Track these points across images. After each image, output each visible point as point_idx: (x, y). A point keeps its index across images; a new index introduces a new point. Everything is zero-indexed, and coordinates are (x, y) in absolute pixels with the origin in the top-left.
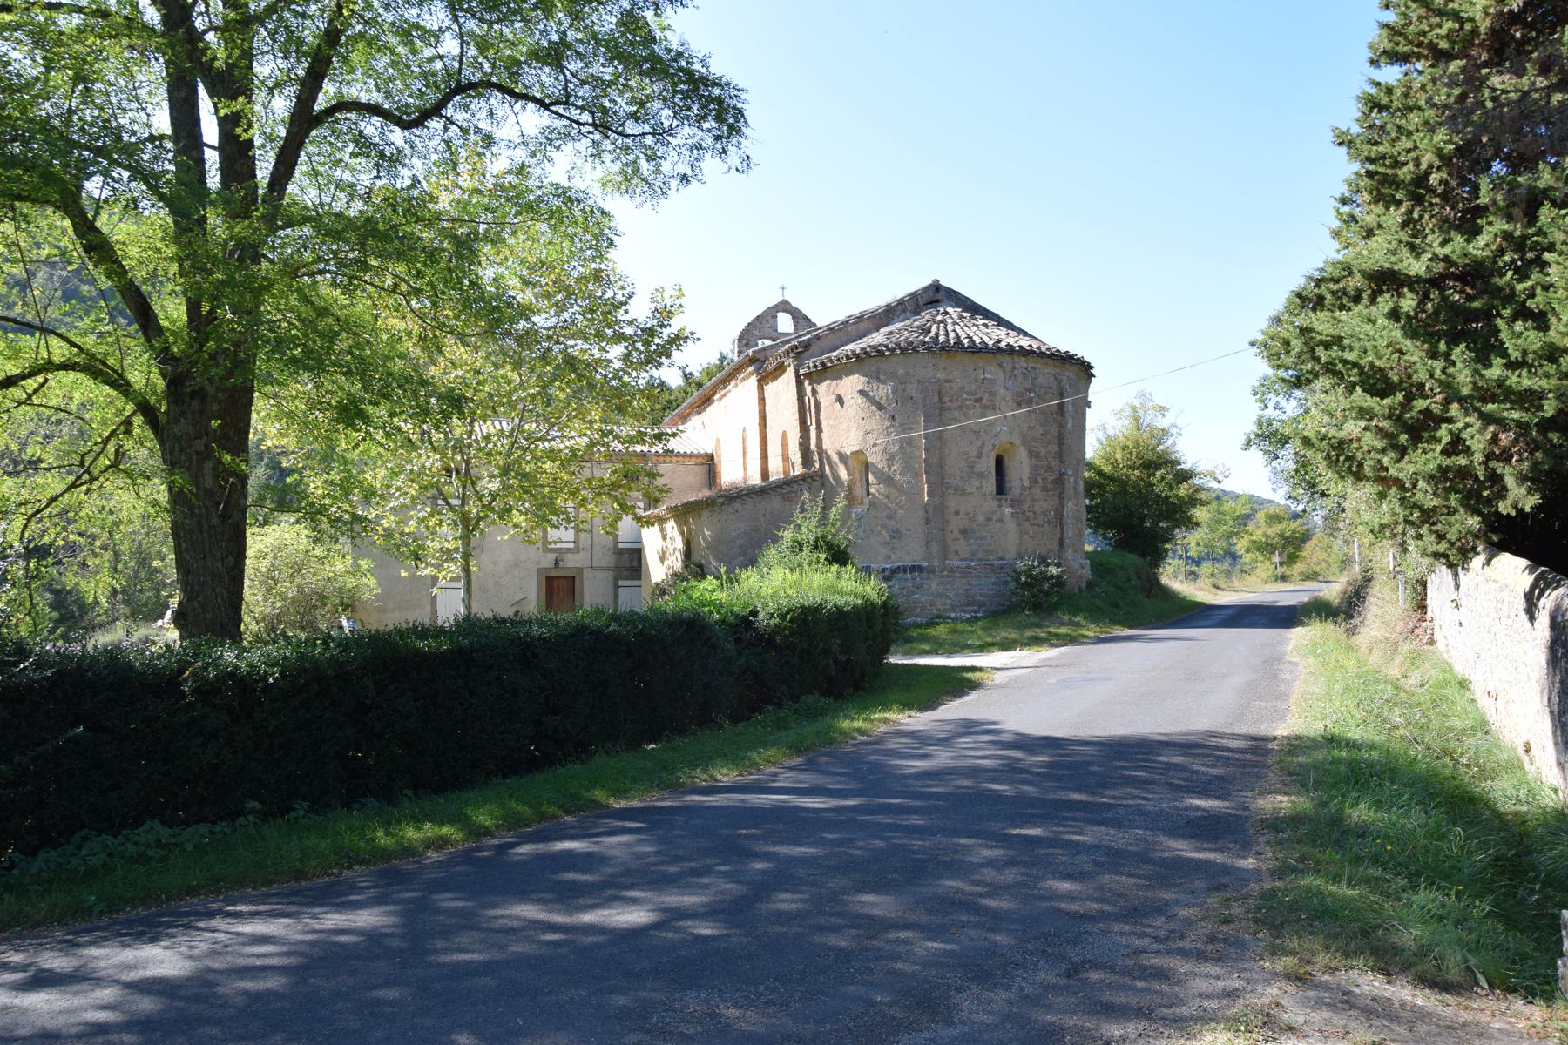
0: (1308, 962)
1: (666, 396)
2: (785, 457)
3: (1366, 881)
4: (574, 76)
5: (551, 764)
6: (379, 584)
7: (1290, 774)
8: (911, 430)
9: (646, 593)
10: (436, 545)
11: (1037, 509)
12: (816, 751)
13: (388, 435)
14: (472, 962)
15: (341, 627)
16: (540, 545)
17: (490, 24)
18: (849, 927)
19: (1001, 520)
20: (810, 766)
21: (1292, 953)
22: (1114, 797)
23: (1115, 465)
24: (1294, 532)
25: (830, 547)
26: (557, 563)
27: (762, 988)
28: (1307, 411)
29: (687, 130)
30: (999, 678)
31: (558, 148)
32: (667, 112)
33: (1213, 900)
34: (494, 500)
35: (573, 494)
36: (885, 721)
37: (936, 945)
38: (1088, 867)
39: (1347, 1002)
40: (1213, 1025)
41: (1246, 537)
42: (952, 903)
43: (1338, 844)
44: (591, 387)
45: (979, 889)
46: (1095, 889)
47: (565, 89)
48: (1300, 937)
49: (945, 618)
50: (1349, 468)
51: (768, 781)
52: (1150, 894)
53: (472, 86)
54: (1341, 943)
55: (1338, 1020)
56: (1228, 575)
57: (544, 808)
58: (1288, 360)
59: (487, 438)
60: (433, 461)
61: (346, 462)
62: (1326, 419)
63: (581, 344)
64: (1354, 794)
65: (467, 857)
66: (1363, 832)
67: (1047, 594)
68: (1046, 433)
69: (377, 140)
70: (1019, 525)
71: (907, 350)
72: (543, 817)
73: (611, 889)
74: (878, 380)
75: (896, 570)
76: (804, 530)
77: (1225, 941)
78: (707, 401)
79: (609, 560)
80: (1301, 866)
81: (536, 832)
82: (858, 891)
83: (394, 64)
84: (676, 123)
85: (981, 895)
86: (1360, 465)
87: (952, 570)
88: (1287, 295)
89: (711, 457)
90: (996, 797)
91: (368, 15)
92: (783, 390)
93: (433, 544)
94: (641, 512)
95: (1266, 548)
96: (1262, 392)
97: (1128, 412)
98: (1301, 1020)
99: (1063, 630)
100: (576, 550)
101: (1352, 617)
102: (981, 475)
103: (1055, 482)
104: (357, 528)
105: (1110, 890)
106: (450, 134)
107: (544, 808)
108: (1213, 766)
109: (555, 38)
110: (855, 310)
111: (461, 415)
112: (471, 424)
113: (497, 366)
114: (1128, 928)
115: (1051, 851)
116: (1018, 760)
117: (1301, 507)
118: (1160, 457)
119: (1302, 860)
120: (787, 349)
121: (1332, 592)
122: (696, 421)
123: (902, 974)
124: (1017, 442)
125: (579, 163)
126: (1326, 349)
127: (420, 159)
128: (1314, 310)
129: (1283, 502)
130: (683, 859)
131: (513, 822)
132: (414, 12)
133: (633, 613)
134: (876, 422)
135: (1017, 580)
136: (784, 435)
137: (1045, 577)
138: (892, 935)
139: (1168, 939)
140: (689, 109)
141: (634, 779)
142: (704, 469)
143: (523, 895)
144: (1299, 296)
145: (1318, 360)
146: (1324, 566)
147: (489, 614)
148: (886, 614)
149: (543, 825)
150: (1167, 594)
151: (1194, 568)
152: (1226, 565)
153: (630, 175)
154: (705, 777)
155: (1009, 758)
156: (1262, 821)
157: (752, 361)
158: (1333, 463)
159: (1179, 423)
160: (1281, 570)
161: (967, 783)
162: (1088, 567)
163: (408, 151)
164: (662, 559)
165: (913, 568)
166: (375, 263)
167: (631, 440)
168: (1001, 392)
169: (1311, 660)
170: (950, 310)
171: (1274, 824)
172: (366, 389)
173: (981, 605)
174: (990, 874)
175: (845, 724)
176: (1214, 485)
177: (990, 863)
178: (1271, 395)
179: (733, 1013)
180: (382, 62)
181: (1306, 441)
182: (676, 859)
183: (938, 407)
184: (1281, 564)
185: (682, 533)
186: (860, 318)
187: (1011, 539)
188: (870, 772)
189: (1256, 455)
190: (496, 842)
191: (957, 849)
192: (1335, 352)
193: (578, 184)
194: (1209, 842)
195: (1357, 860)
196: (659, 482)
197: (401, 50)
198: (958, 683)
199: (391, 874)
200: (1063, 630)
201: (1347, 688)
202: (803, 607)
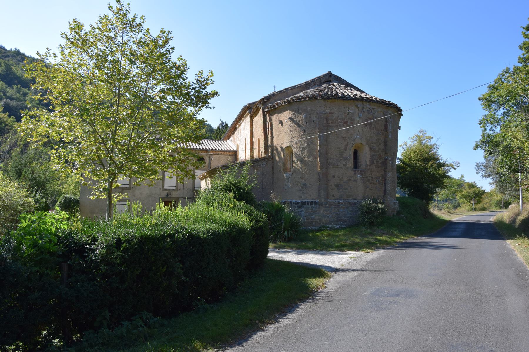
19: (355, 181)
23: (411, 160)
26: (167, 195)
70: (364, 183)
71: (312, 98)
74: (298, 113)
75: (303, 203)
92: (259, 119)
96: (483, 123)
99: (384, 238)
102: (346, 159)
124: (364, 143)
137: (376, 209)
159: (438, 143)
162: (397, 204)
165: (312, 203)
170: (335, 84)
186: (294, 87)
187: (360, 190)
200: (384, 238)
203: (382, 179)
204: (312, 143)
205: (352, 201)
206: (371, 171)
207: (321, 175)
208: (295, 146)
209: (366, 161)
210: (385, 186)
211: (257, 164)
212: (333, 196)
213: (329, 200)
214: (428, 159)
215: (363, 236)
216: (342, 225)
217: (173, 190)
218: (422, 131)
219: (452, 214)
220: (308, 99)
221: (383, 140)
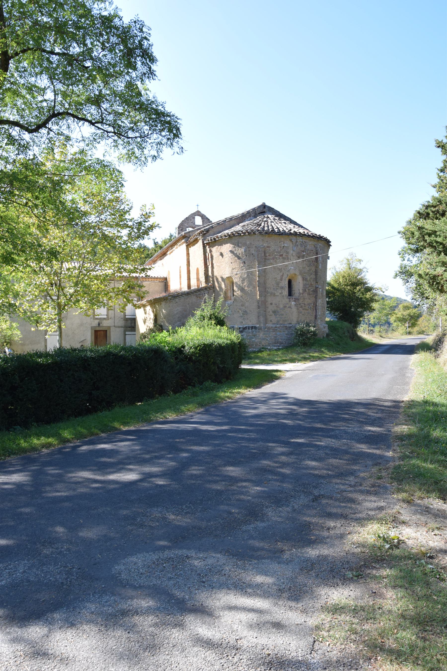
0: (412, 495)
1: (146, 252)
2: (198, 279)
3: (438, 461)
4: (105, 110)
5: (96, 411)
6: (22, 333)
7: (409, 416)
8: (252, 268)
9: (138, 338)
10: (47, 316)
11: (306, 303)
12: (208, 406)
13: (24, 268)
14: (61, 496)
15: (5, 352)
16: (92, 317)
17: (68, 86)
18: (221, 481)
19: (290, 307)
20: (207, 412)
21: (406, 491)
22: (335, 426)
23: (339, 284)
24: (415, 313)
25: (216, 318)
26: (99, 324)
27: (184, 507)
28: (421, 262)
29: (155, 136)
30: (288, 375)
31: (99, 143)
32: (147, 127)
33: (374, 470)
34: (71, 297)
35: (106, 295)
36: (239, 393)
37: (258, 488)
38: (323, 455)
39: (427, 511)
40: (372, 521)
41: (394, 315)
42: (265, 470)
43: (427, 446)
44: (114, 248)
45: (277, 465)
46: (325, 465)
47: (101, 116)
48: (409, 485)
49: (265, 349)
50: (438, 287)
51: (189, 419)
52: (348, 467)
53: (59, 114)
54: (426, 487)
55: (423, 519)
56: (387, 331)
57: (92, 430)
58: (413, 241)
59: (68, 269)
60: (45, 280)
61: (6, 281)
62: (429, 266)
63: (110, 229)
64: (434, 425)
65: (60, 451)
66: (437, 441)
67: (309, 339)
68: (310, 270)
69: (17, 138)
70: (298, 309)
71: (251, 233)
72: (92, 434)
73: (121, 465)
74: (238, 246)
75: (245, 328)
76: (205, 311)
77: (379, 486)
78: (164, 254)
79: (122, 323)
80: (411, 455)
81: (89, 441)
82: (225, 465)
83: (25, 103)
84: (150, 132)
85: (277, 467)
86: (442, 286)
87: (269, 328)
88: (414, 212)
89: (166, 279)
90: (285, 426)
91: (12, 80)
92: (197, 250)
93: (45, 317)
94: (135, 302)
95: (402, 320)
96: (402, 254)
97: (345, 261)
98: (408, 519)
99: (316, 354)
100: (107, 319)
101: (437, 350)
102: (282, 288)
103: (313, 291)
104: (11, 310)
105: (332, 465)
106: (50, 136)
107: (92, 430)
108: (377, 413)
109: (97, 93)
110: (229, 215)
111: (56, 258)
112: (62, 264)
113: (72, 239)
114: (338, 481)
115: (307, 449)
116: (295, 410)
117: (418, 303)
118: (359, 281)
119: (412, 453)
120: (199, 232)
121: (430, 339)
122: (159, 263)
123: (243, 500)
124: (298, 273)
125: (108, 149)
126: (429, 237)
127: (37, 147)
128: (425, 219)
129: (410, 301)
130: (152, 452)
131: (79, 436)
132: (33, 79)
133: (131, 347)
134: (237, 264)
135: (297, 332)
136: (198, 270)
138: (240, 484)
139: (355, 486)
140: (156, 126)
141: (131, 418)
142: (163, 284)
143: (84, 467)
144: (419, 213)
145: (426, 241)
146: (427, 328)
147: (69, 347)
148: (240, 347)
149: (92, 438)
150: (360, 339)
151: (372, 328)
152: (386, 327)
153: (130, 156)
154: (162, 417)
155: (291, 409)
156: (396, 436)
157: (184, 237)
158: (431, 285)
160: (408, 330)
161: (273, 420)
163: (32, 144)
164: (145, 322)
165: (252, 328)
166: (17, 193)
167: (131, 271)
168: (291, 252)
169: (420, 368)
170: (270, 216)
171: (401, 438)
172: (15, 247)
173: (281, 343)
174: (283, 458)
175: (222, 394)
176: (382, 293)
177: (283, 454)
178: (406, 255)
179: (172, 517)
180: (19, 102)
181: (420, 276)
182: (149, 452)
183: (264, 258)
184: (409, 327)
185: (153, 312)
186: (231, 219)
187: (294, 315)
188: (232, 415)
189: (399, 281)
190: (72, 445)
191: (267, 448)
192: (433, 238)
193: (108, 159)
194: (362, 451)
195: (435, 453)
196: (144, 289)
197: (28, 96)
198: (270, 377)
199: (27, 459)
201: (434, 380)
202: (204, 344)
203: (313, 305)
204: (251, 274)
205: (288, 325)
206: (304, 299)
207: (260, 303)
208: (236, 276)
209: (299, 290)
210: (316, 311)
211: (199, 293)
212: (271, 321)
213: (267, 325)
214: (356, 283)
215: (299, 354)
216: (279, 346)
217: (104, 319)
218: (351, 254)
219: (384, 338)
220: (247, 234)
221: (314, 270)
